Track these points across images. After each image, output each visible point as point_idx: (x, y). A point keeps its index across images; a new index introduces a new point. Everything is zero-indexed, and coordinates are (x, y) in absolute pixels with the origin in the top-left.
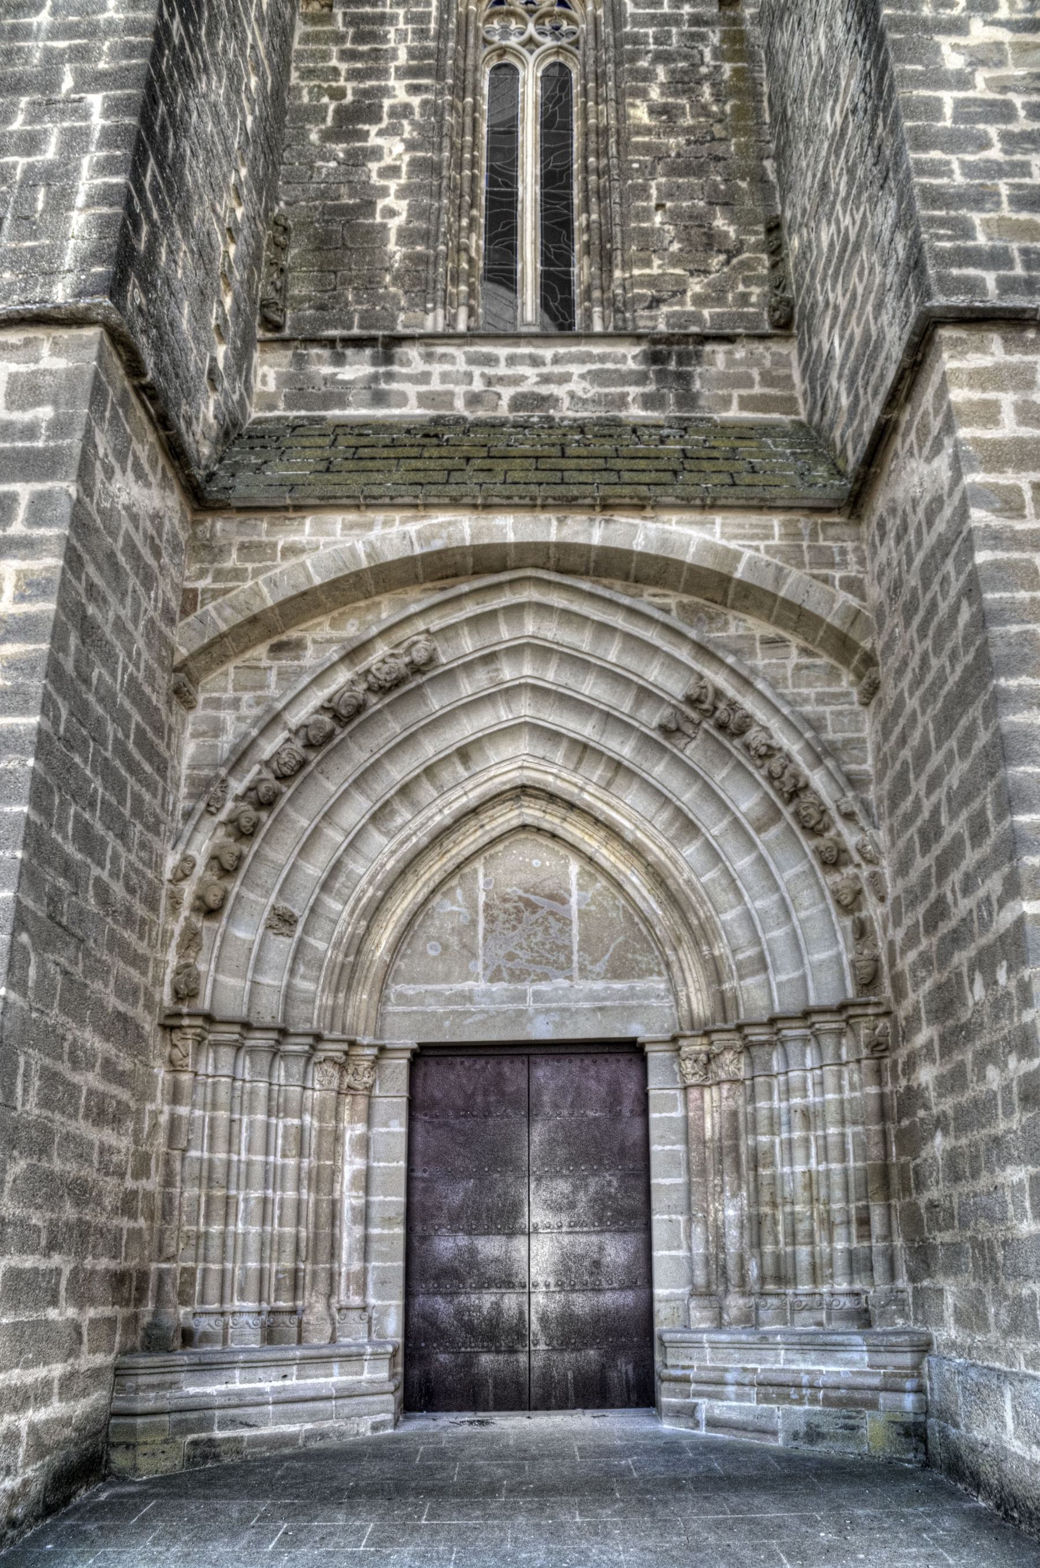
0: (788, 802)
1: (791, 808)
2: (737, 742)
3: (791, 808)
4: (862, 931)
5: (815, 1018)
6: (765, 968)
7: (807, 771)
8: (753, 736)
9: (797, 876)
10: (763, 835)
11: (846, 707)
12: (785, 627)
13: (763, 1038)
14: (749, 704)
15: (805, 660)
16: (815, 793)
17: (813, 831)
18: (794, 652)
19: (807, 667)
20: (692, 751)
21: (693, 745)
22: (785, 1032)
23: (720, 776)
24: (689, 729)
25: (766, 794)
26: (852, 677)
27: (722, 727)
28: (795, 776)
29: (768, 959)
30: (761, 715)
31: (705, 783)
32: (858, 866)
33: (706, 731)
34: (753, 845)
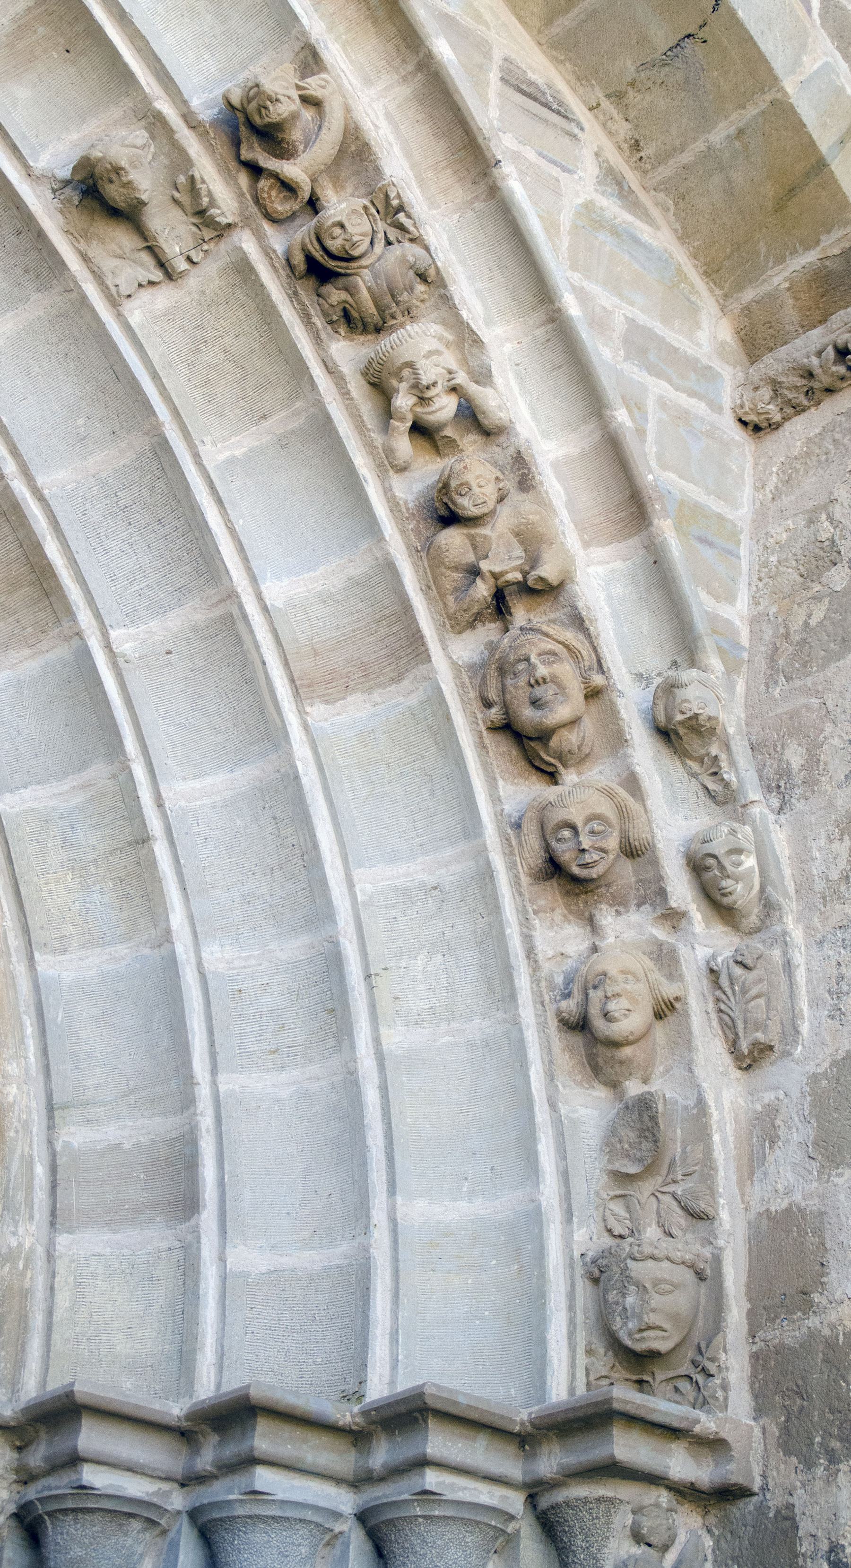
0: (461, 622)
1: (469, 647)
2: (348, 352)
3: (469, 647)
4: (645, 1144)
5: (439, 1442)
6: (188, 1205)
7: (572, 540)
8: (420, 341)
9: (405, 894)
10: (317, 711)
11: (700, 408)
12: (582, 78)
13: (136, 1487)
14: (446, 230)
15: (610, 206)
16: (579, 622)
17: (530, 745)
18: (589, 170)
19: (615, 232)
20: (159, 323)
21: (164, 298)
22: (264, 1478)
23: (227, 451)
24: (171, 230)
25: (389, 567)
26: (726, 332)
27: (320, 269)
28: (531, 541)
29: (208, 1172)
30: (475, 286)
31: (162, 448)
32: (673, 918)
33: (243, 269)
34: (273, 736)
